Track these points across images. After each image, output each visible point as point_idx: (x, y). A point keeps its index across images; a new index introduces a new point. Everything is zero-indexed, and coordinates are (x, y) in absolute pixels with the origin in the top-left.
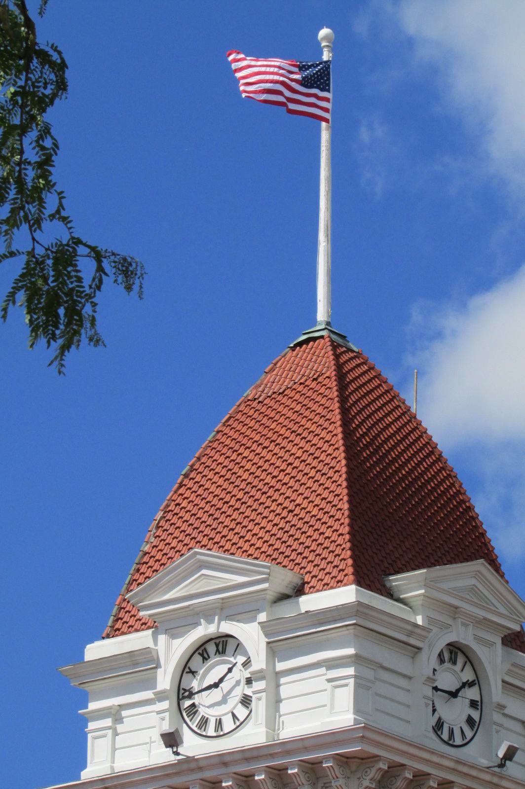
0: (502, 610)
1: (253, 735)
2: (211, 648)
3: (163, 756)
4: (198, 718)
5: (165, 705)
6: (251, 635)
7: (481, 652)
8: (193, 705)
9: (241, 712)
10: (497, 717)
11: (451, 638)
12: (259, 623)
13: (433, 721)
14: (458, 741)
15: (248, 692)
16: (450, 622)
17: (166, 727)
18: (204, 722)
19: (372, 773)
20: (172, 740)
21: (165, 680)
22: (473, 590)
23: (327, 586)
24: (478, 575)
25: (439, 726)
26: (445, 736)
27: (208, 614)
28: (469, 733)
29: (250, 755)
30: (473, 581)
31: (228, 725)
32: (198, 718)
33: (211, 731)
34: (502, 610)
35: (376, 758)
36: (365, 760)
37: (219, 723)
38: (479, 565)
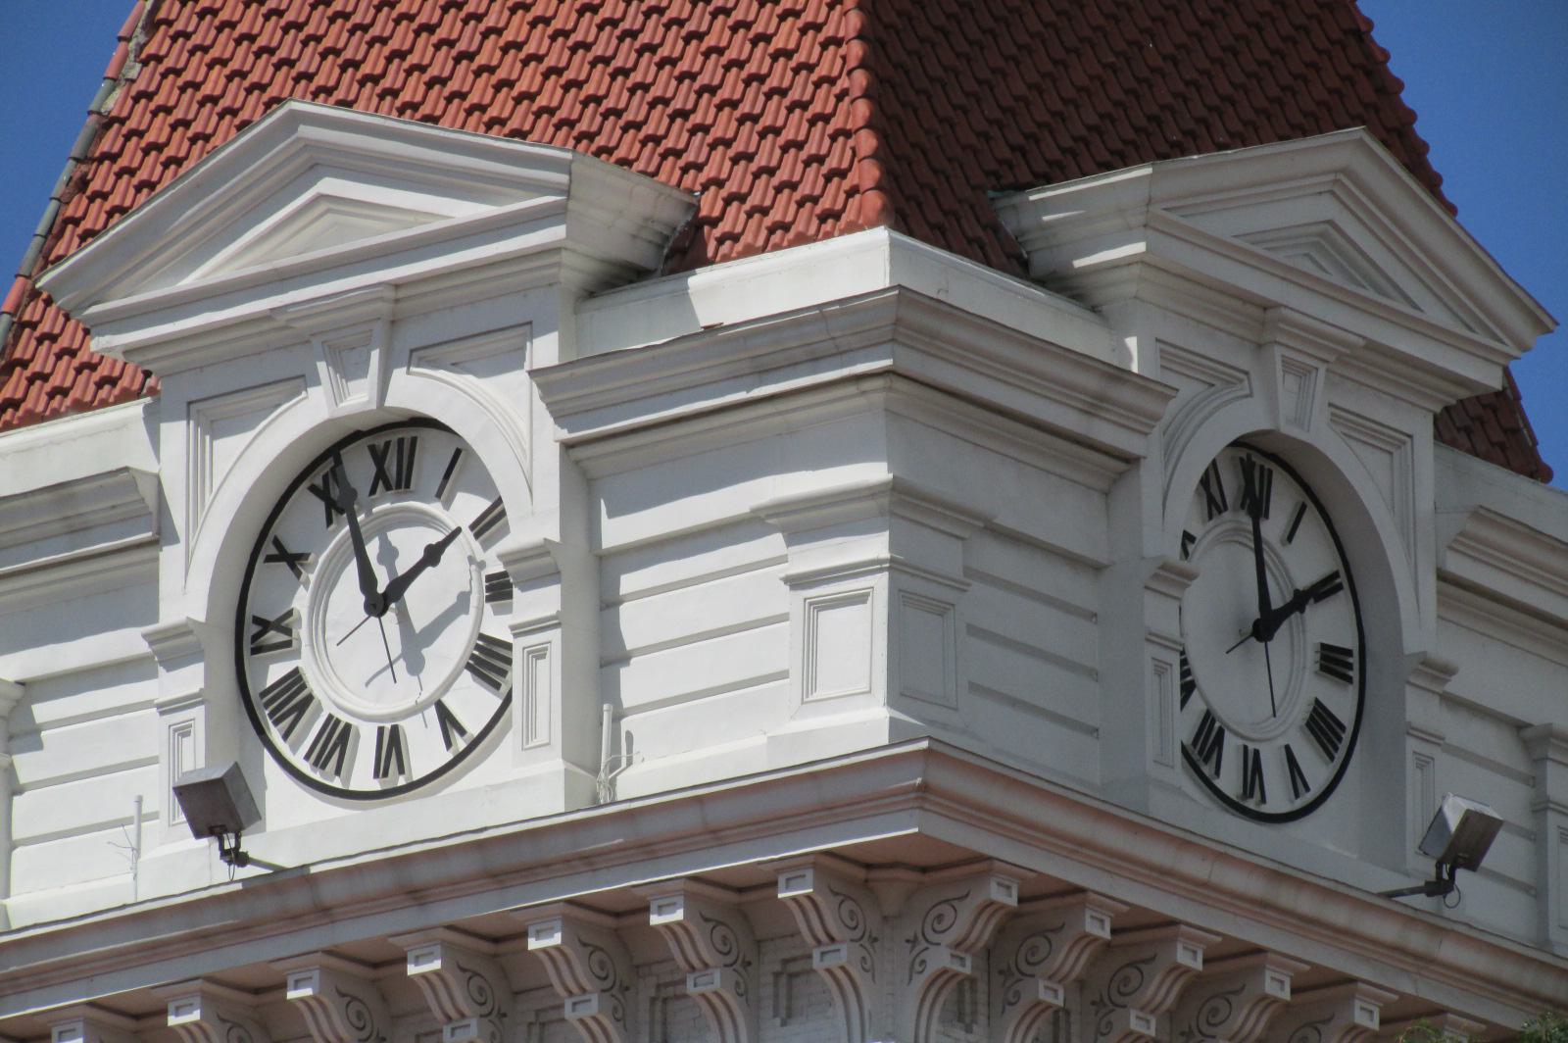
0: (1435, 314)
1: (520, 785)
2: (359, 468)
3: (184, 866)
4: (311, 730)
5: (190, 679)
6: (500, 415)
7: (1362, 472)
8: (295, 679)
9: (473, 704)
10: (1420, 709)
11: (1246, 417)
12: (533, 373)
13: (1184, 726)
14: (1278, 797)
15: (497, 627)
16: (1243, 360)
17: (196, 761)
18: (336, 741)
19: (962, 921)
20: (217, 808)
21: (188, 587)
22: (1326, 239)
23: (781, 234)
24: (1342, 185)
25: (1207, 742)
26: (1230, 781)
27: (339, 341)
28: (1317, 770)
29: (508, 858)
30: (1328, 208)
31: (425, 750)
32: (311, 730)
33: (362, 775)
34: (1435, 314)
35: (976, 865)
36: (935, 872)
37: (391, 746)
38: (1347, 149)
